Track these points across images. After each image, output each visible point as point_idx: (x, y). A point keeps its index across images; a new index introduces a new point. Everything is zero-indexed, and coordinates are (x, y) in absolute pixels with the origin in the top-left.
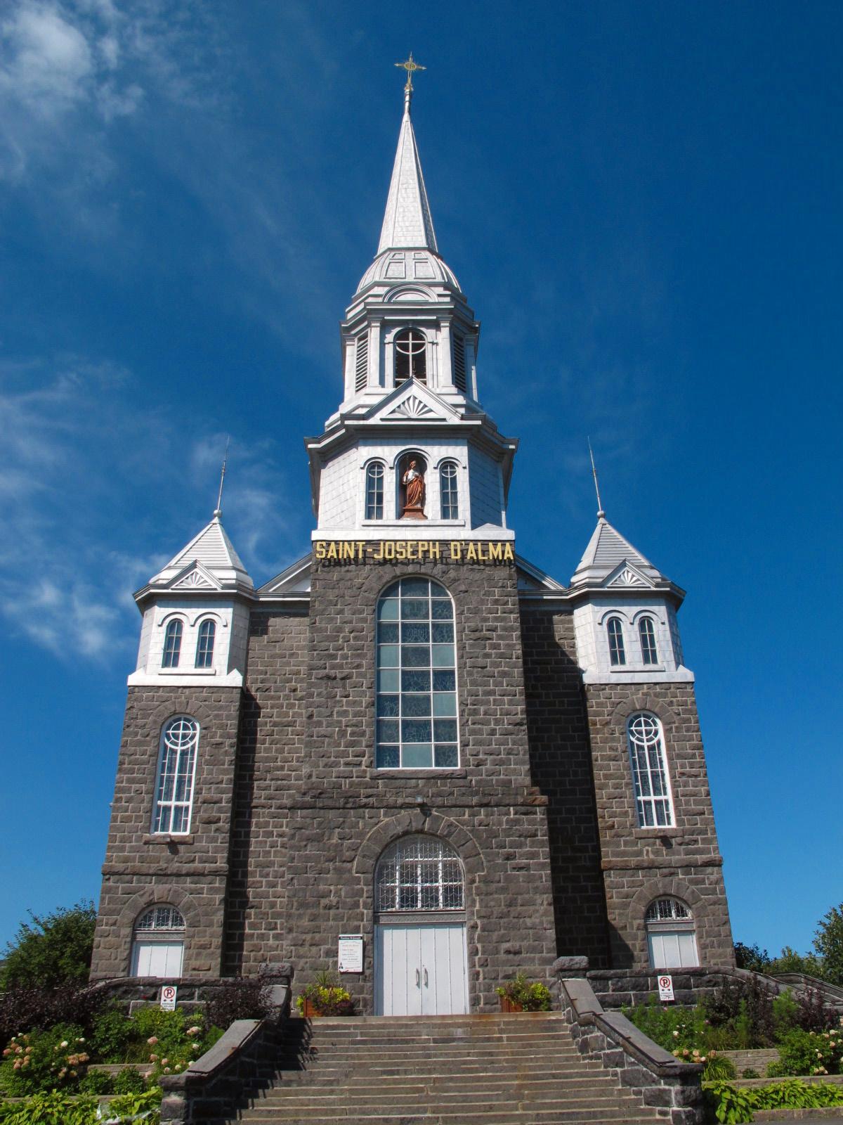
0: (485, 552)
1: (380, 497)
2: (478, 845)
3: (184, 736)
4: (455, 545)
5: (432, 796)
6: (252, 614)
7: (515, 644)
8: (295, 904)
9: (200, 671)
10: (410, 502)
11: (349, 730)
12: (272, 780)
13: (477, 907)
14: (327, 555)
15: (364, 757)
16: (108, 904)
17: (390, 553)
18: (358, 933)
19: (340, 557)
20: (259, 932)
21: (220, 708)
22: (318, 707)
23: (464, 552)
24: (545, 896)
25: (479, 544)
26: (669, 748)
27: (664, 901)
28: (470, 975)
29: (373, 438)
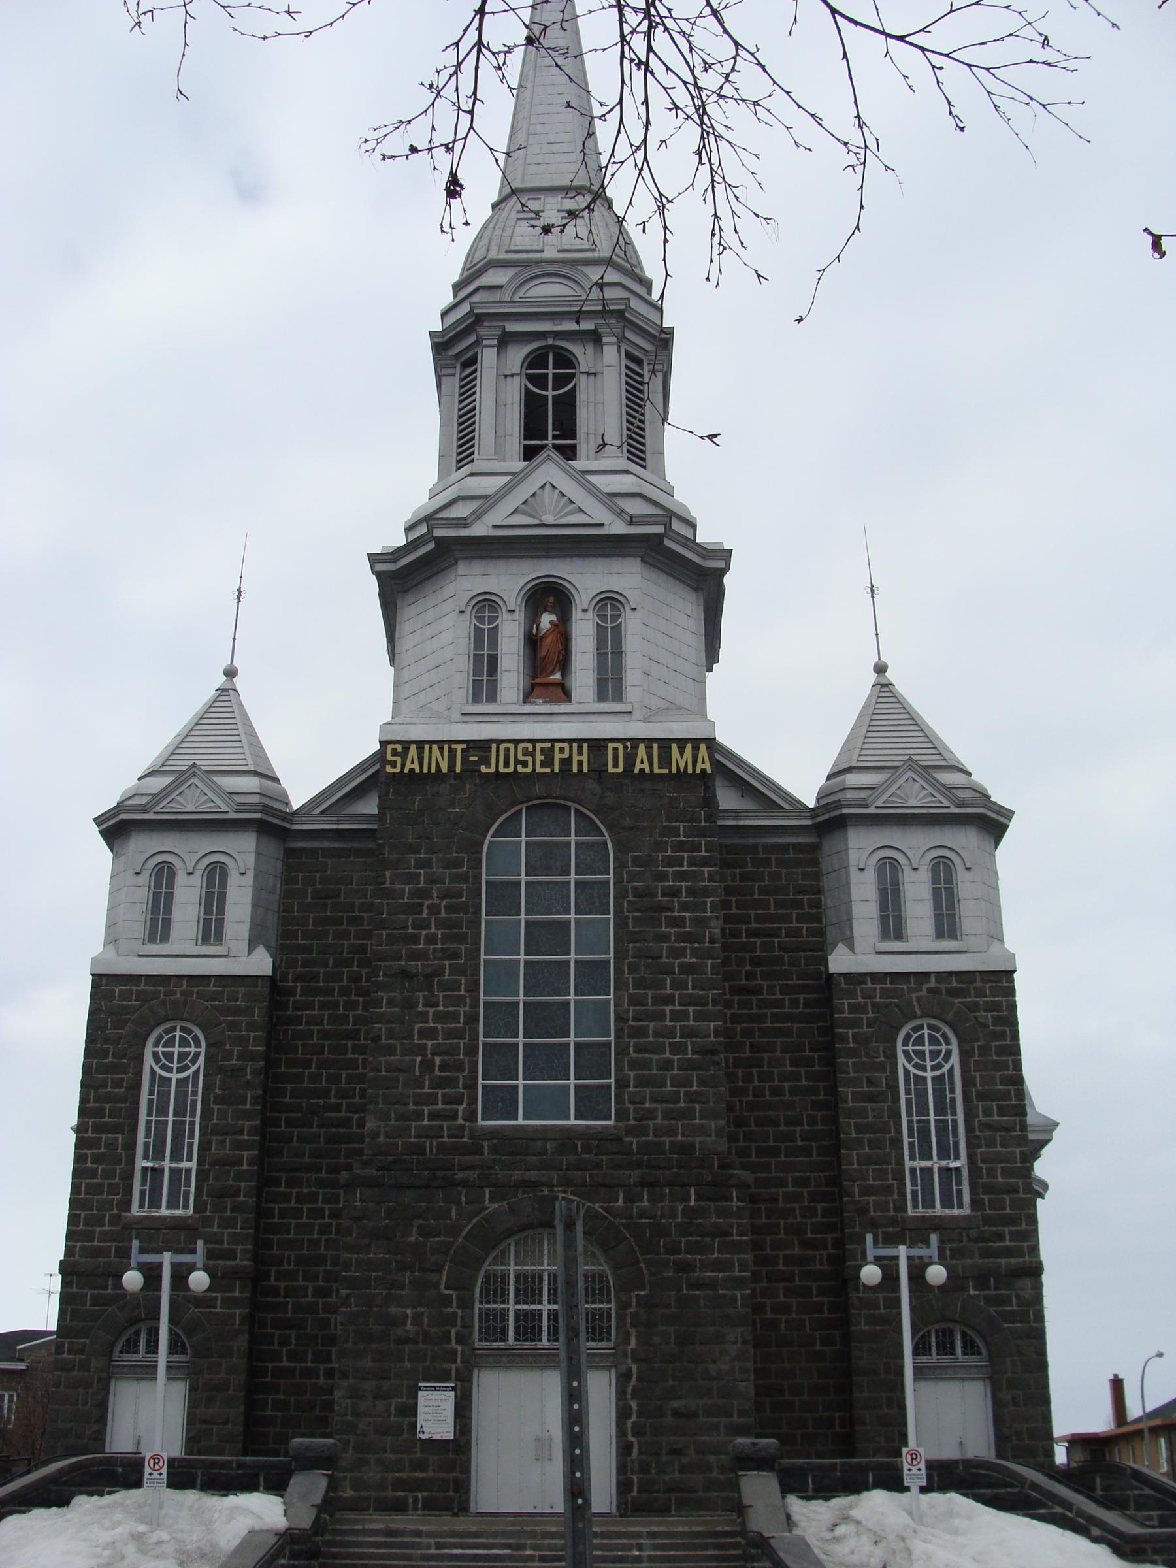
0: (665, 760)
1: (493, 662)
2: (636, 1248)
3: (182, 1056)
4: (616, 749)
5: (567, 1169)
6: (289, 853)
7: (709, 918)
8: (352, 1335)
9: (205, 950)
10: (547, 668)
11: (438, 1060)
12: (320, 1126)
13: (633, 1343)
14: (403, 766)
15: (461, 1104)
16: (71, 1320)
17: (506, 765)
18: (448, 1380)
19: (425, 770)
20: (304, 1365)
21: (237, 1011)
22: (389, 1022)
23: (630, 759)
24: (740, 1330)
25: (655, 746)
26: (967, 1082)
27: (944, 1330)
28: (618, 1447)
29: (482, 558)
